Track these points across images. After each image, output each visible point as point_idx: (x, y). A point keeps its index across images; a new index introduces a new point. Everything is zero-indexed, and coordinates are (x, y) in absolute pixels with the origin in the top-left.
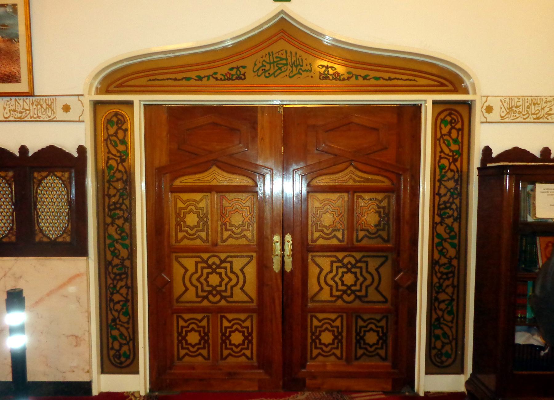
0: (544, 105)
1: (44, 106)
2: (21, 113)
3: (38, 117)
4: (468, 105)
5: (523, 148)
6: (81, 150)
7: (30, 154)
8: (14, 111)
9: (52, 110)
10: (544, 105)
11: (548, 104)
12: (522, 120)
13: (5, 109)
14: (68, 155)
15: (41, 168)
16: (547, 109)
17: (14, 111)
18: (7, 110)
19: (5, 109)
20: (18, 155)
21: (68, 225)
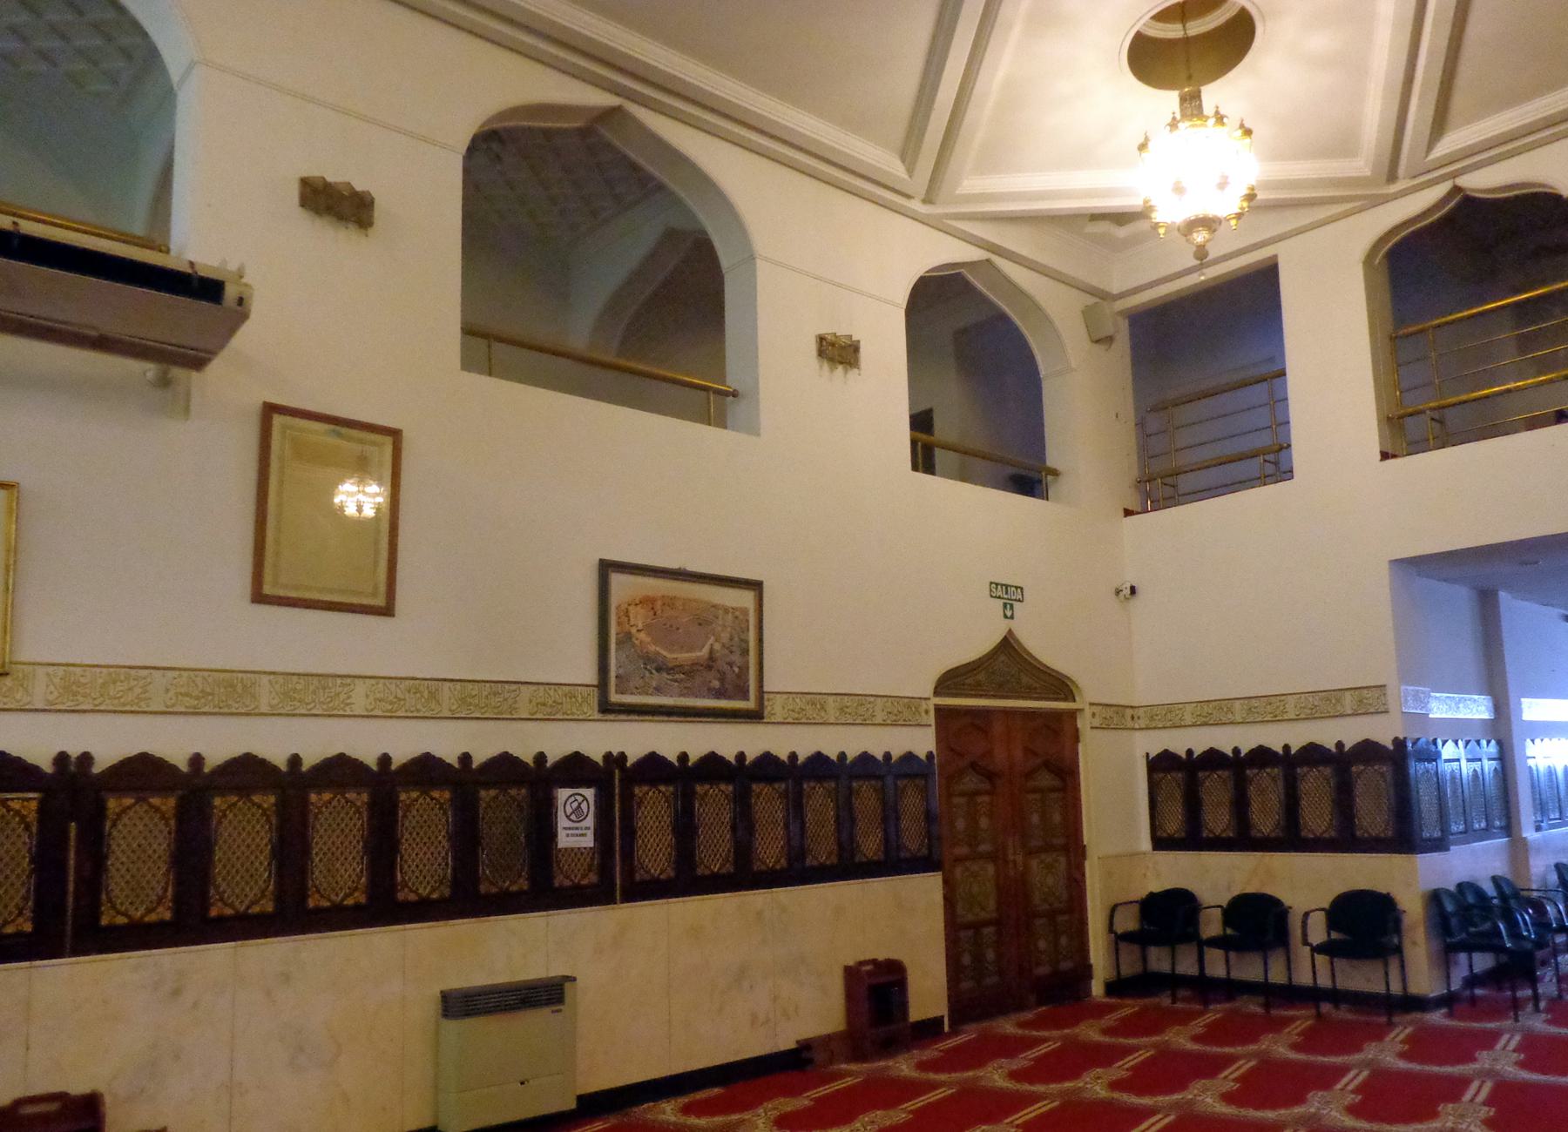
0: (133, 683)
1: (426, 694)
2: (391, 703)
3: (229, 706)
4: (1073, 715)
5: (15, 754)
6: (930, 755)
7: (393, 767)
8: (187, 695)
9: (26, 690)
10: (133, 683)
11: (142, 683)
12: (90, 707)
13: (167, 690)
14: (1275, 754)
15: (1204, 769)
16: (138, 690)
17: (187, 695)
18: (171, 693)
19: (167, 690)
20: (375, 768)
21: (166, 890)
